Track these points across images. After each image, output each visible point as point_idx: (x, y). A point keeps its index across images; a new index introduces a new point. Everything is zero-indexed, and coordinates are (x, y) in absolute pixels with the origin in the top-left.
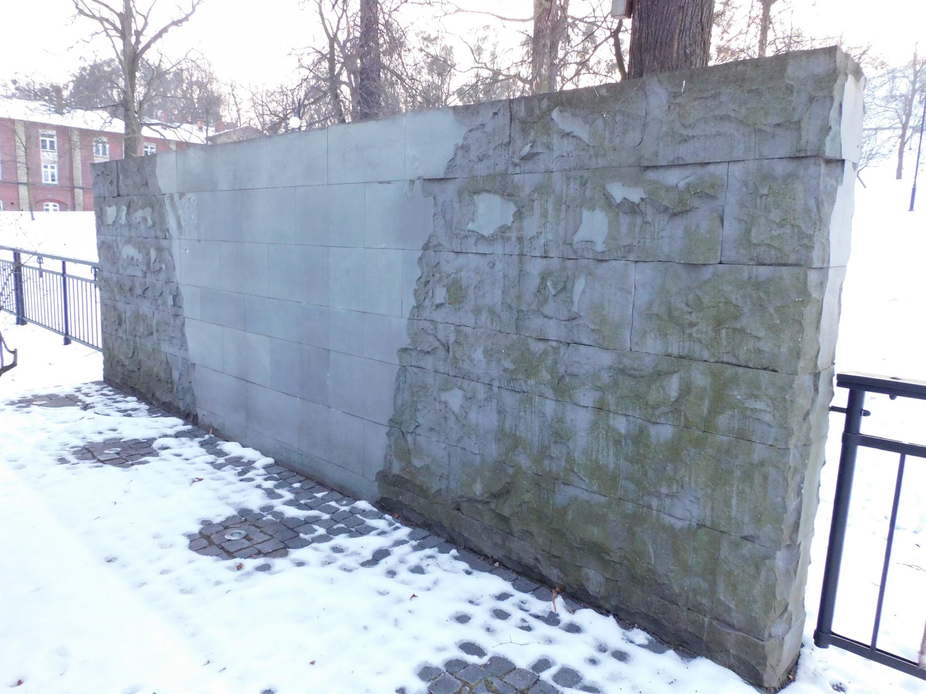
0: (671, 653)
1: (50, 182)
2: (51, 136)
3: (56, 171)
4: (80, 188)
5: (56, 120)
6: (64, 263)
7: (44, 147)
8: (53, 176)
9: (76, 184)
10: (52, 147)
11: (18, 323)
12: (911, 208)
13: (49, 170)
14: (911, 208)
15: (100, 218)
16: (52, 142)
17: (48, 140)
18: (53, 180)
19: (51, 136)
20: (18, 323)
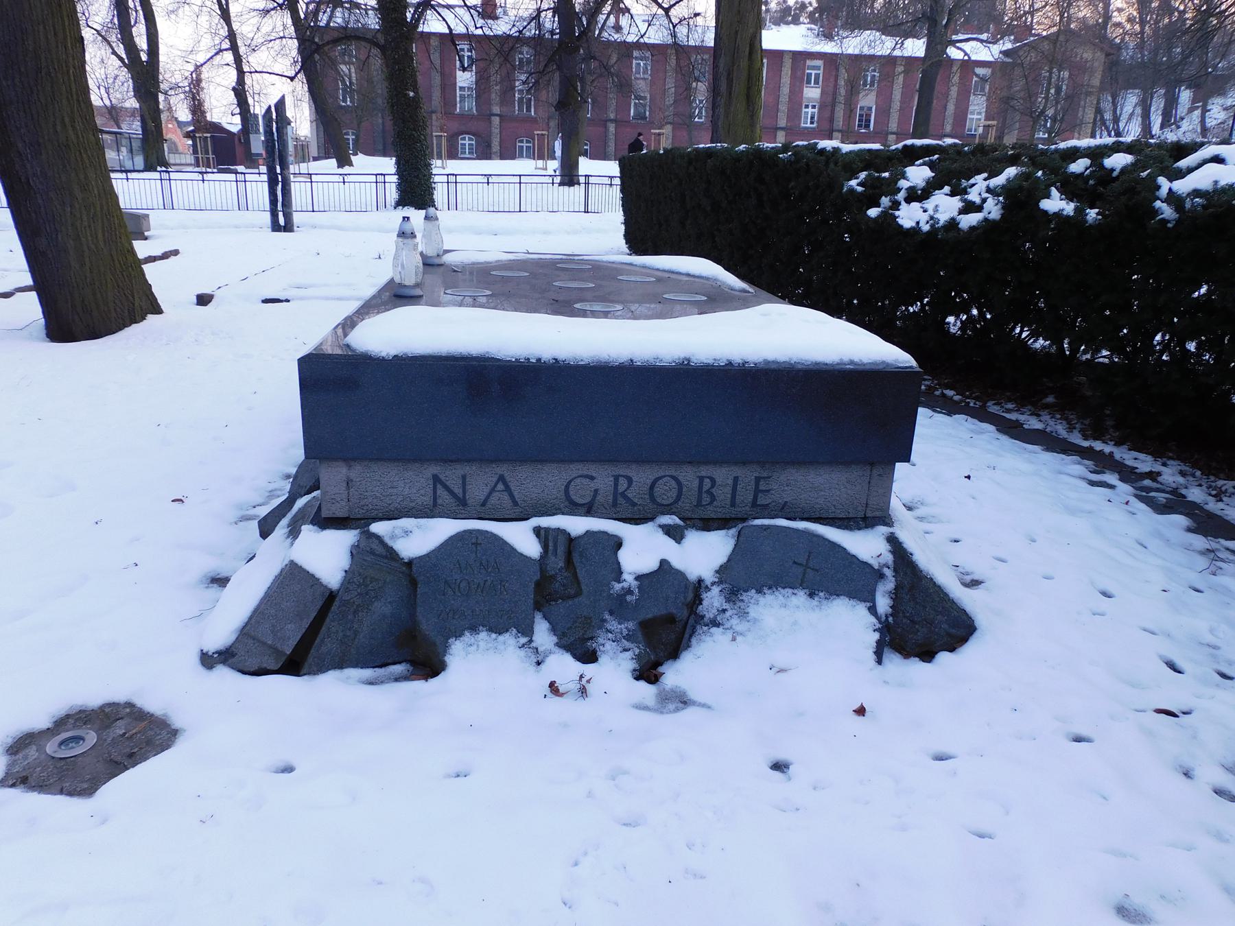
0: (483, 635)
1: (809, 125)
2: (817, 68)
3: (816, 110)
4: (838, 131)
5: (829, 47)
6: (586, 204)
7: (809, 82)
8: (812, 118)
9: (835, 127)
10: (816, 82)
11: (62, 327)
12: (266, 301)
13: (810, 110)
14: (266, 301)
15: (585, 154)
16: (817, 76)
17: (813, 72)
18: (812, 123)
19: (817, 68)
20: (62, 327)
